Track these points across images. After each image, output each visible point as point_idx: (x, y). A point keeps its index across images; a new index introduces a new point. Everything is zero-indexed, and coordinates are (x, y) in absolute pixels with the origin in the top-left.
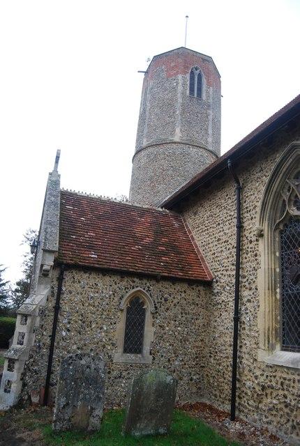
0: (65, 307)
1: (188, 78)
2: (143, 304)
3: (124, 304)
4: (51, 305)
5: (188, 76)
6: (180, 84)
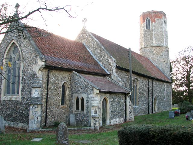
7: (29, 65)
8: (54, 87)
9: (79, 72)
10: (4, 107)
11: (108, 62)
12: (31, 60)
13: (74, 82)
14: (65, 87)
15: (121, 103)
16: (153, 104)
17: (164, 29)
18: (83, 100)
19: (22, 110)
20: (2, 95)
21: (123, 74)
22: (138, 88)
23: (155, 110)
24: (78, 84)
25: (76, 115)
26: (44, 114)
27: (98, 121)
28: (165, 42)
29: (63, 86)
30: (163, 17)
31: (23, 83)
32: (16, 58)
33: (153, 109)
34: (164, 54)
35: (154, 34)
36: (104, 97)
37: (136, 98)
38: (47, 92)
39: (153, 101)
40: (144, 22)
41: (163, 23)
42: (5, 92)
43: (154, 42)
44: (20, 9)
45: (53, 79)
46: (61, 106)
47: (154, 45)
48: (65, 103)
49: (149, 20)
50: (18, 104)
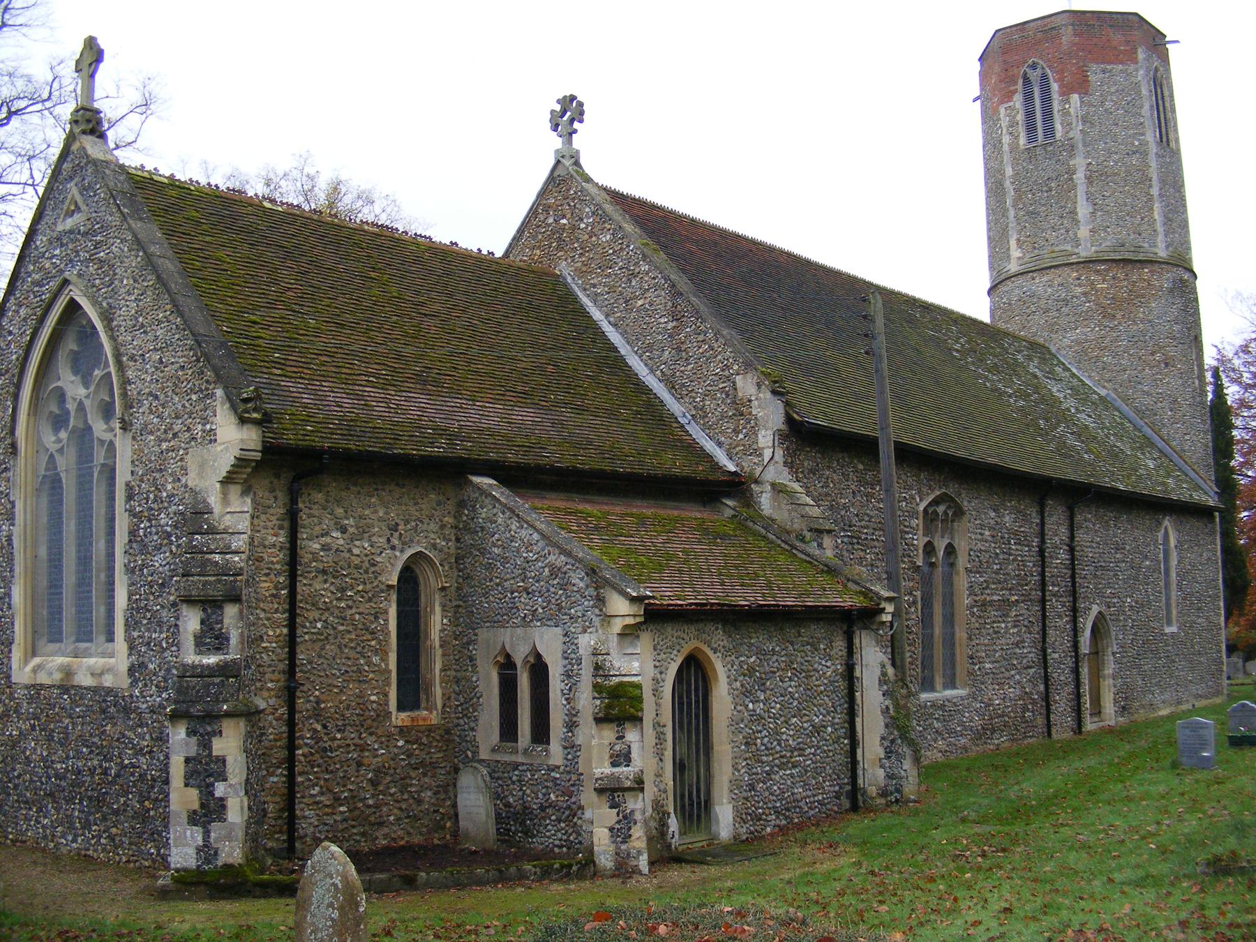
5: (1018, 101)
7: (164, 446)
8: (343, 590)
9: (523, 478)
10: (33, 727)
11: (731, 392)
12: (177, 417)
13: (483, 552)
14: (422, 587)
15: (820, 684)
16: (1085, 671)
17: (1151, 137)
18: (539, 670)
19: (139, 752)
20: (17, 654)
21: (841, 477)
22: (962, 561)
23: (1097, 712)
24: (506, 560)
25: (498, 773)
26: (277, 779)
27: (638, 816)
28: (1160, 229)
29: (409, 577)
30: (1141, 55)
31: (133, 572)
32: (87, 403)
33: (1087, 700)
34: (1160, 309)
35: (1080, 176)
36: (686, 651)
37: (950, 641)
38: (292, 626)
39: (1085, 648)
40: (1009, 96)
41: (1144, 92)
42: (34, 632)
43: (1083, 232)
44: (104, 74)
45: (327, 534)
46: (400, 718)
47: (1086, 251)
48: (423, 696)
49: (1044, 77)
50: (112, 710)
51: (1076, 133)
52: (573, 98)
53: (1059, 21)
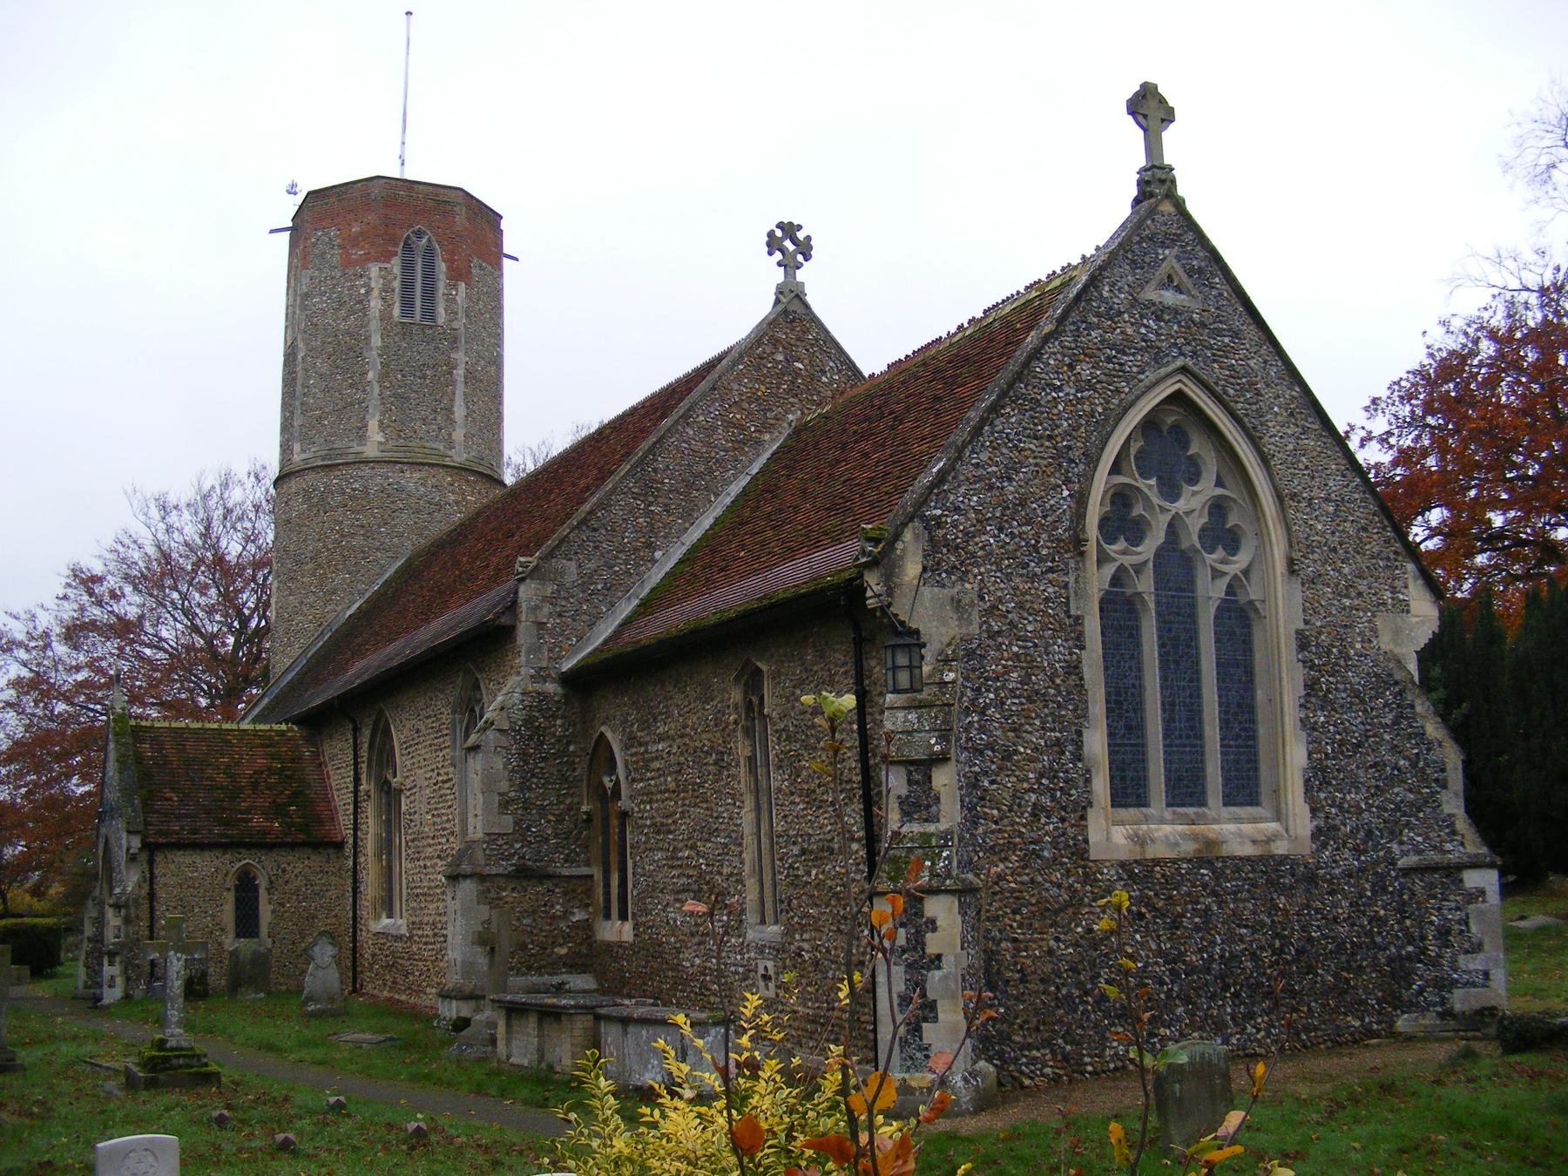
0: (162, 894)
1: (397, 270)
2: (255, 878)
3: (231, 882)
4: (145, 891)
5: (396, 265)
6: (375, 293)
35: (460, 372)
43: (458, 435)
47: (459, 456)
51: (460, 323)
52: (771, 234)
53: (452, 196)
